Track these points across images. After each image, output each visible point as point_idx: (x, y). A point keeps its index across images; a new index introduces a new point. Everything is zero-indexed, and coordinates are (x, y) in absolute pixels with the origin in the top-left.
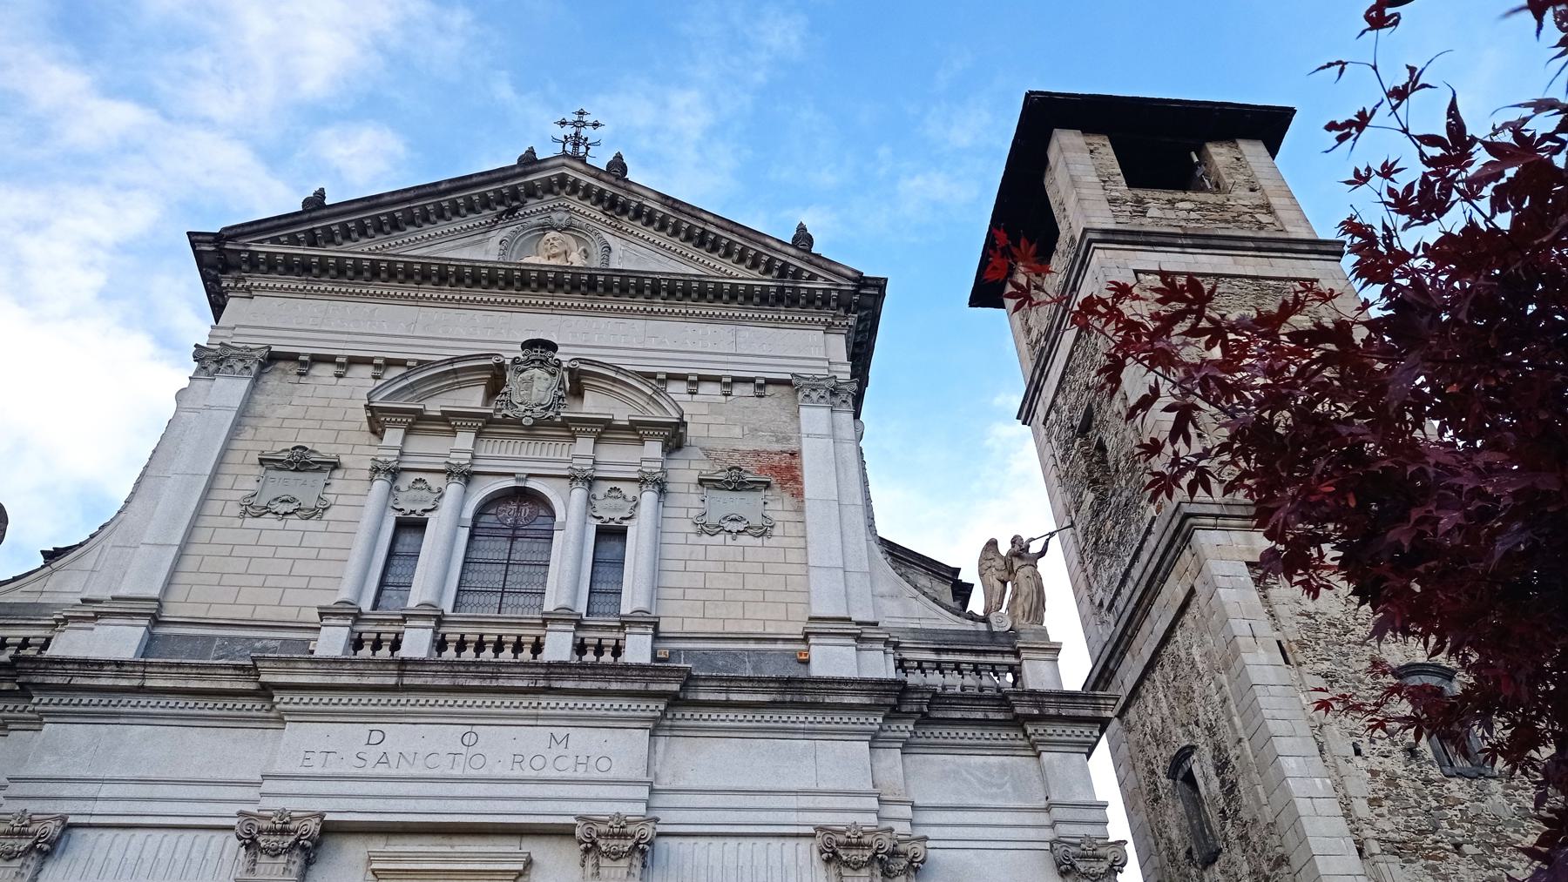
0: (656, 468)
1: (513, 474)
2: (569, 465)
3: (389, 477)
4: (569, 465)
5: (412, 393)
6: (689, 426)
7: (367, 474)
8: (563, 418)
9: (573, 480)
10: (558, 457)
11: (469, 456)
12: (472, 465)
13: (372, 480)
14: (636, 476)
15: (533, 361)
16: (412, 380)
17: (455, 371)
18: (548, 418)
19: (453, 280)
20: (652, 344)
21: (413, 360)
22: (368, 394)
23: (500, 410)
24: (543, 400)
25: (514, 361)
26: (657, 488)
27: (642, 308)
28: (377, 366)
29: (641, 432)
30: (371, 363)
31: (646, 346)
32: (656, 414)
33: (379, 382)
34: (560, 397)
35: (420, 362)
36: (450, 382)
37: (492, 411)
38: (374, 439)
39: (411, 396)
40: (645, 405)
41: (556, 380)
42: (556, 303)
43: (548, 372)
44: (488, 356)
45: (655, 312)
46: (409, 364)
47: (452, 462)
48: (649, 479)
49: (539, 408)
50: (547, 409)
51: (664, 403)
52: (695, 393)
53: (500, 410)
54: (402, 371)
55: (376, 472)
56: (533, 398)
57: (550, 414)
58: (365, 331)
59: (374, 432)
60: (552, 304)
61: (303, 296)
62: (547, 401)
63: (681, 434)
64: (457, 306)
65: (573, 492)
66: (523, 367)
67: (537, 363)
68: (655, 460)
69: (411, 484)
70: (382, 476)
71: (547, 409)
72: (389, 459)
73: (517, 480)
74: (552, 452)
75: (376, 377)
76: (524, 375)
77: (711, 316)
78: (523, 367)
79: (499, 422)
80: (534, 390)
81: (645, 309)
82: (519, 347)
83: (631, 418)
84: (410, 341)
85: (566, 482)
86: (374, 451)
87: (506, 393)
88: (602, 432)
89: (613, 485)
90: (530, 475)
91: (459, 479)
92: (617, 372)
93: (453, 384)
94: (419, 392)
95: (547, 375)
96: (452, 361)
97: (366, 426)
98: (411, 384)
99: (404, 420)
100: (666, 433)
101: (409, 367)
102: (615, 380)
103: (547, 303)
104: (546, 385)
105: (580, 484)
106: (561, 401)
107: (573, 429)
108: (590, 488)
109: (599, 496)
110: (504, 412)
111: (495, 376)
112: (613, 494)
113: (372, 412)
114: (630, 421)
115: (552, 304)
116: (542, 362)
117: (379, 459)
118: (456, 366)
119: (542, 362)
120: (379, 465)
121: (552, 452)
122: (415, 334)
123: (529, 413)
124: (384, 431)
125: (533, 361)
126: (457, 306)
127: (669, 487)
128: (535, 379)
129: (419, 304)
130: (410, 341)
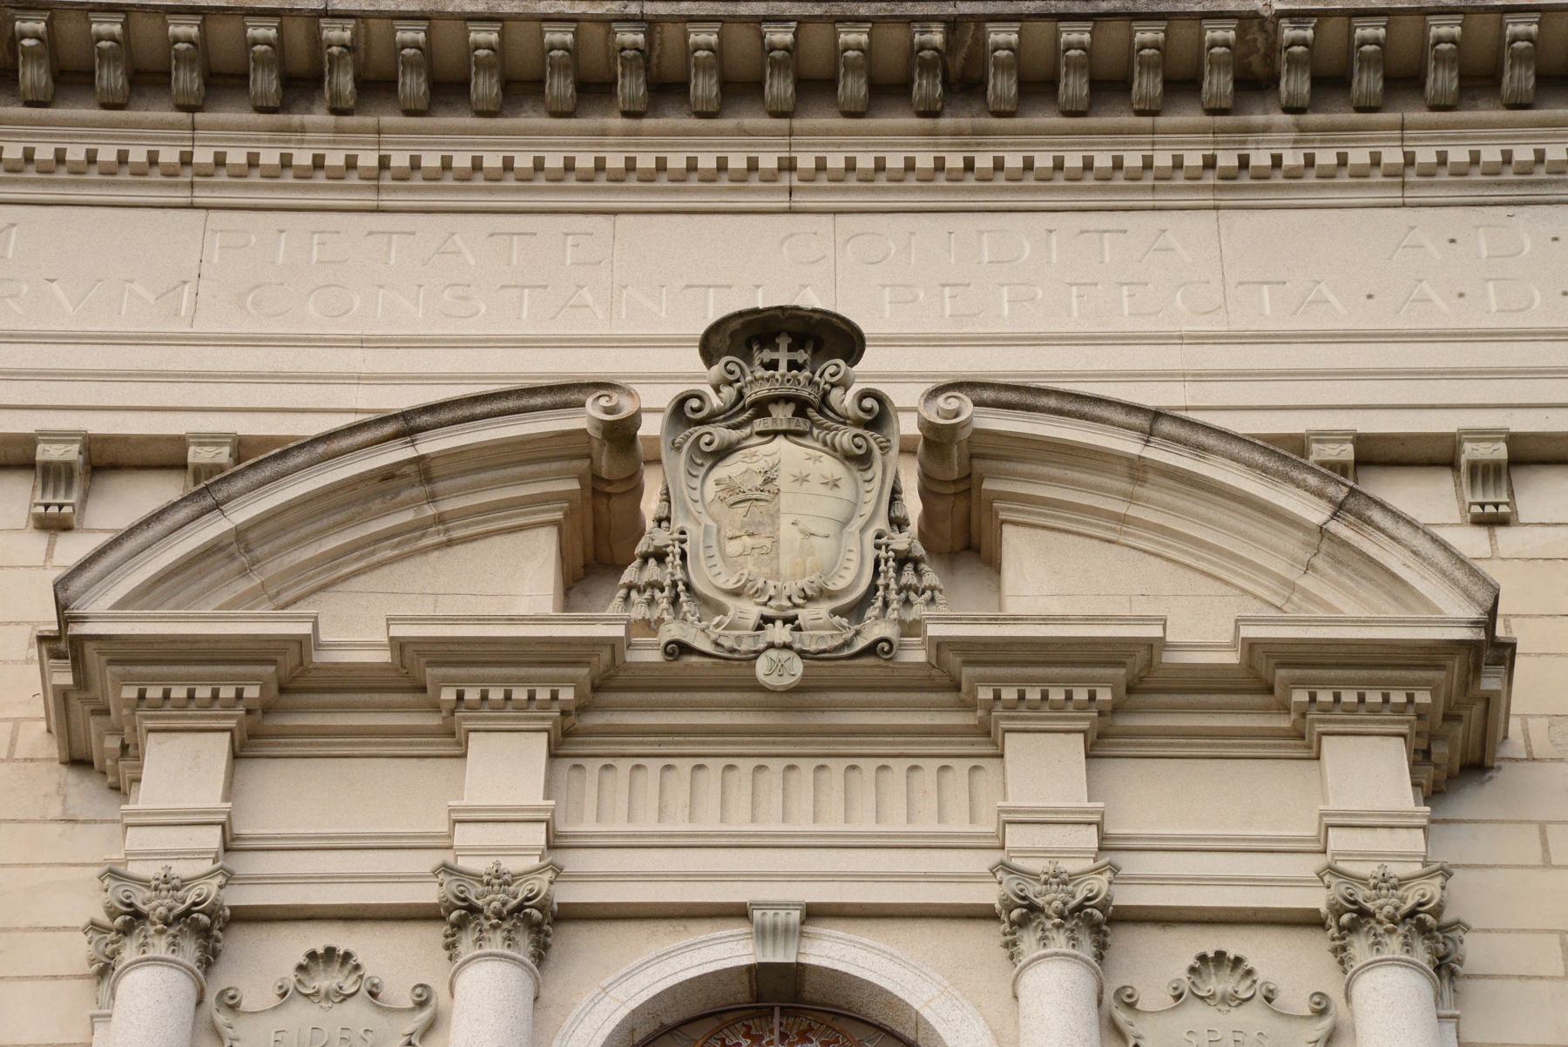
0: (1402, 857)
1: (739, 912)
2: (437, 858)
3: (190, 951)
4: (437, 858)
5: (244, 572)
6: (1522, 665)
7: (79, 951)
8: (940, 644)
9: (460, 925)
10: (868, 825)
11: (538, 835)
12: (230, 878)
13: (105, 971)
14: (428, 894)
15: (762, 408)
16: (242, 513)
17: (423, 469)
18: (871, 650)
19: (345, 82)
20: (1267, 312)
21: (214, 440)
22: (61, 585)
23: (651, 626)
24: (830, 570)
25: (681, 414)
26: (1421, 955)
27: (1193, 159)
28: (55, 475)
29: (1300, 696)
30: (1451, 463)
31: (1240, 325)
32: (1351, 609)
33: (72, 549)
34: (903, 560)
35: (243, 448)
36: (407, 517)
37: (618, 631)
38: (83, 792)
39: (243, 586)
40: (1294, 575)
41: (873, 496)
42: (806, 161)
43: (833, 449)
44: (565, 393)
45: (1261, 175)
46: (197, 455)
47: (463, 863)
48: (1383, 905)
49: (822, 609)
50: (856, 611)
51: (1394, 560)
52: (1502, 521)
53: (651, 626)
54: (166, 489)
55: (126, 930)
56: (786, 563)
57: (876, 628)
58: (118, 327)
59: (79, 761)
60: (788, 166)
61: (181, 197)
62: (851, 577)
63: (1488, 700)
64: (369, 199)
65: (463, 981)
66: (720, 434)
67: (782, 416)
68: (1390, 823)
69: (291, 977)
70: (160, 947)
71: (856, 611)
72: (182, 869)
73: (763, 934)
74: (928, 805)
75: (53, 525)
76: (731, 468)
77: (1525, 169)
78: (720, 434)
79: (648, 684)
80: (786, 531)
81: (1210, 163)
82: (692, 359)
83: (400, 631)
84: (186, 359)
85: (988, 938)
86: (98, 846)
87: (660, 556)
88: (582, 709)
89: (1210, 941)
90: (814, 913)
91: (509, 941)
92: (1148, 435)
93: (421, 527)
94: (273, 567)
95: (831, 466)
96: (408, 424)
97: (37, 737)
98: (240, 533)
99: (1398, 697)
100: (1423, 697)
101: (200, 472)
102: (1137, 469)
103: (768, 161)
104: (831, 505)
105: (1060, 942)
106: (908, 577)
107: (985, 694)
108: (209, 959)
109: (1152, 995)
110: (673, 631)
111: (597, 487)
112: (325, 980)
113: (79, 666)
114: (399, 645)
115: (788, 166)
116: (801, 407)
117: (134, 869)
118: (430, 445)
119: (801, 407)
120: (140, 898)
121: (928, 805)
122: (199, 328)
123: (780, 633)
124: (129, 751)
125: (762, 408)
126: (369, 199)
127: (1474, 952)
128: (783, 482)
129: (202, 196)
130: (186, 359)
